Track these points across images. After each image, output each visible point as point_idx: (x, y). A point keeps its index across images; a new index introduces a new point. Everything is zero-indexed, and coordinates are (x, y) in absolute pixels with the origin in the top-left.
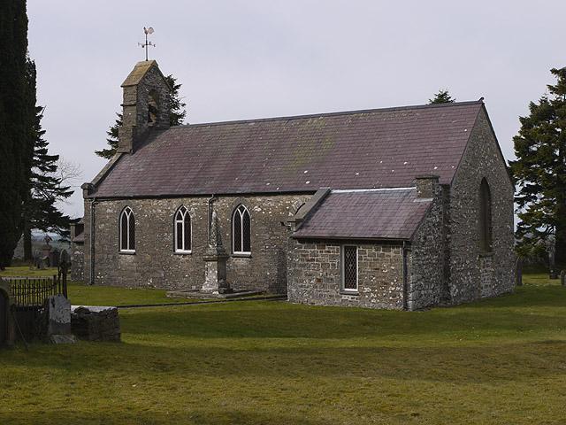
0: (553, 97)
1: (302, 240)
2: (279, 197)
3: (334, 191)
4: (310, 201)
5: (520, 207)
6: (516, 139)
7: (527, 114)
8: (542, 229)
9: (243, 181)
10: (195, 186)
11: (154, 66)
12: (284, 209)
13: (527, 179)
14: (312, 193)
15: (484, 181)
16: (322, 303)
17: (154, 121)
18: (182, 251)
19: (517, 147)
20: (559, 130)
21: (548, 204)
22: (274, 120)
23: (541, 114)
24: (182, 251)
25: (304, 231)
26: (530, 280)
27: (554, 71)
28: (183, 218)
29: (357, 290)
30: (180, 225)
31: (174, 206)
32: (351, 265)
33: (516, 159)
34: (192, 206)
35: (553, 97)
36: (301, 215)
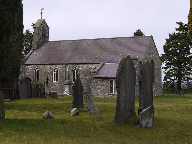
0: (177, 32)
1: (96, 78)
2: (88, 65)
3: (106, 63)
4: (99, 66)
5: (165, 70)
6: (164, 46)
7: (168, 38)
8: (172, 78)
9: (76, 60)
10: (60, 61)
11: (44, 22)
12: (89, 68)
13: (168, 61)
14: (99, 63)
15: (152, 60)
16: (103, 97)
17: (44, 39)
18: (55, 82)
19: (164, 49)
20: (179, 43)
21: (175, 69)
22: (85, 40)
23: (173, 37)
24: (55, 82)
25: (97, 75)
26: (166, 95)
27: (177, 23)
28: (56, 71)
29: (113, 93)
30: (55, 73)
31: (53, 67)
32: (112, 86)
33: (164, 53)
34: (59, 68)
35: (177, 32)
36: (96, 70)
